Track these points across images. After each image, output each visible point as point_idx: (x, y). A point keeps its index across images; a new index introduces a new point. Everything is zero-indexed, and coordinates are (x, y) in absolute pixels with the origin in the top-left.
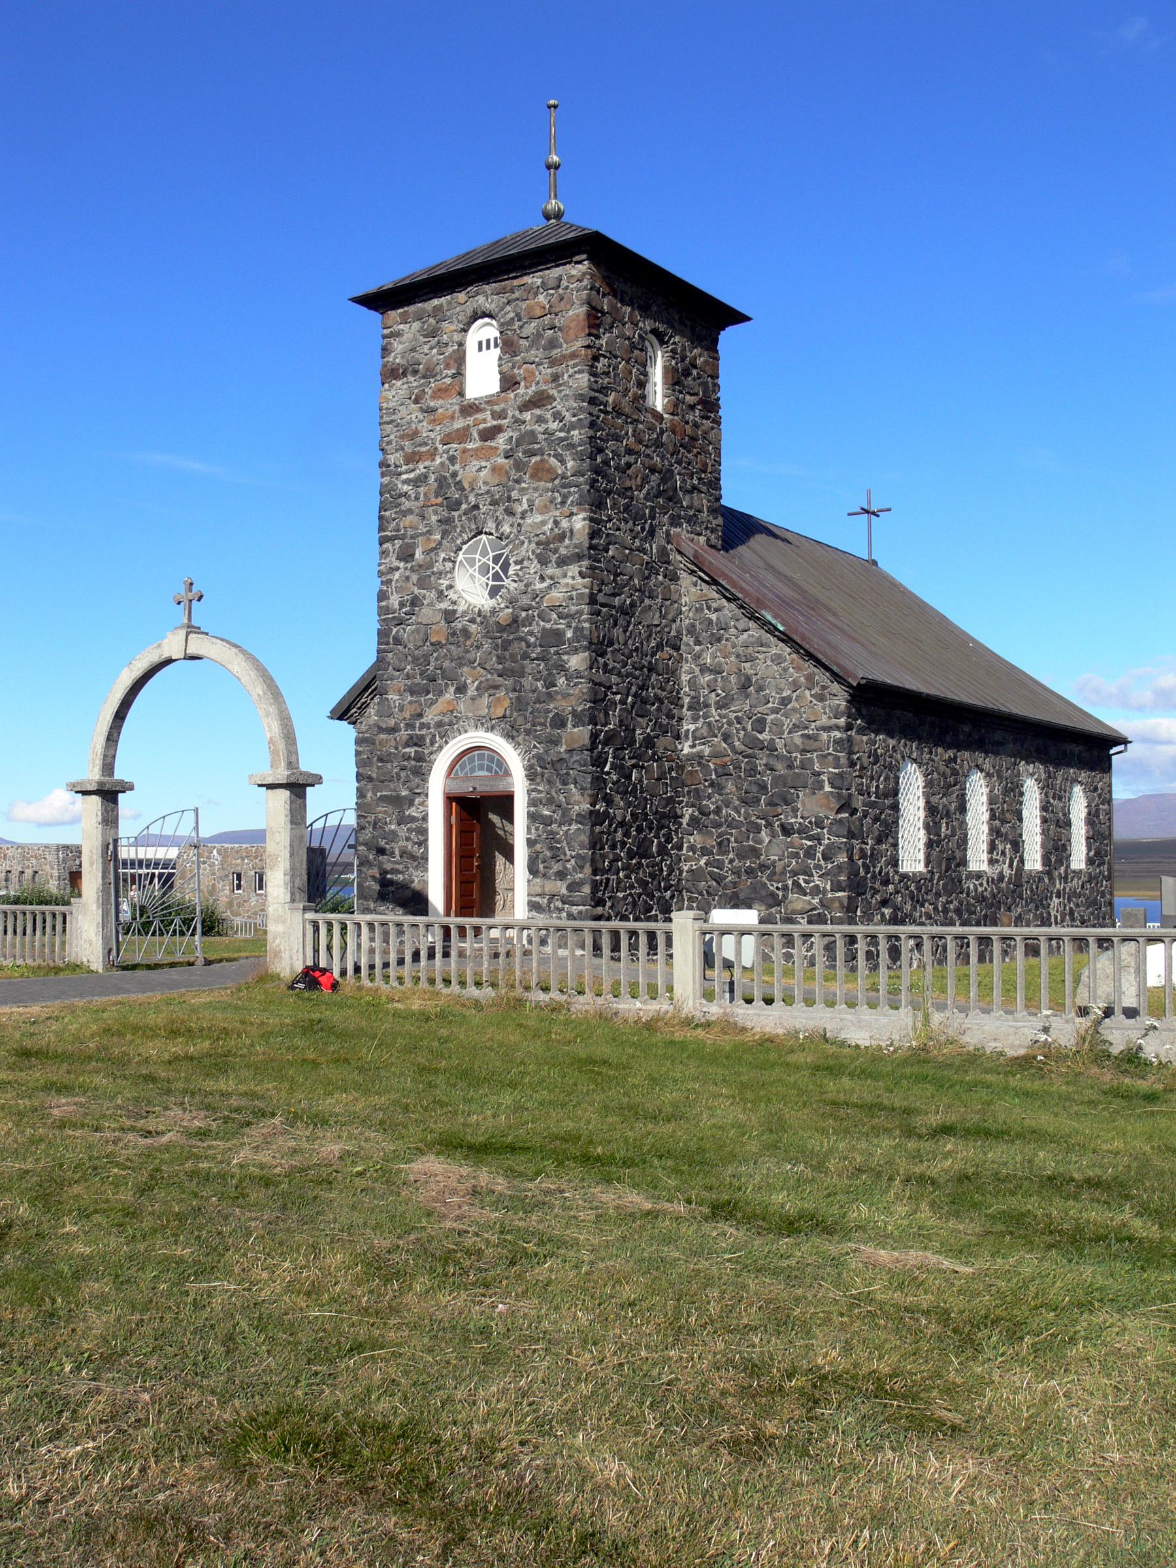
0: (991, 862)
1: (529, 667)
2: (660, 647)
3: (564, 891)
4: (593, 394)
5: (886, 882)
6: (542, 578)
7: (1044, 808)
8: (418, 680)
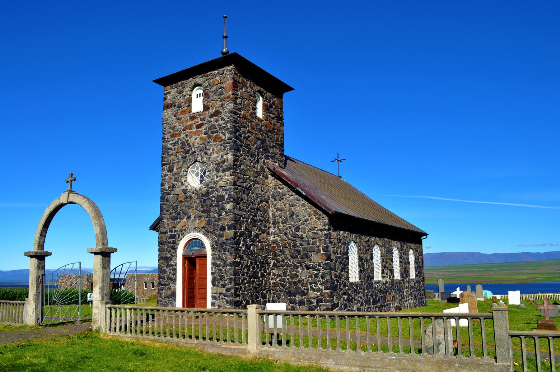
0: (383, 277)
1: (212, 209)
2: (261, 202)
3: (224, 292)
4: (235, 111)
5: (345, 286)
6: (217, 177)
7: (400, 258)
8: (174, 214)
